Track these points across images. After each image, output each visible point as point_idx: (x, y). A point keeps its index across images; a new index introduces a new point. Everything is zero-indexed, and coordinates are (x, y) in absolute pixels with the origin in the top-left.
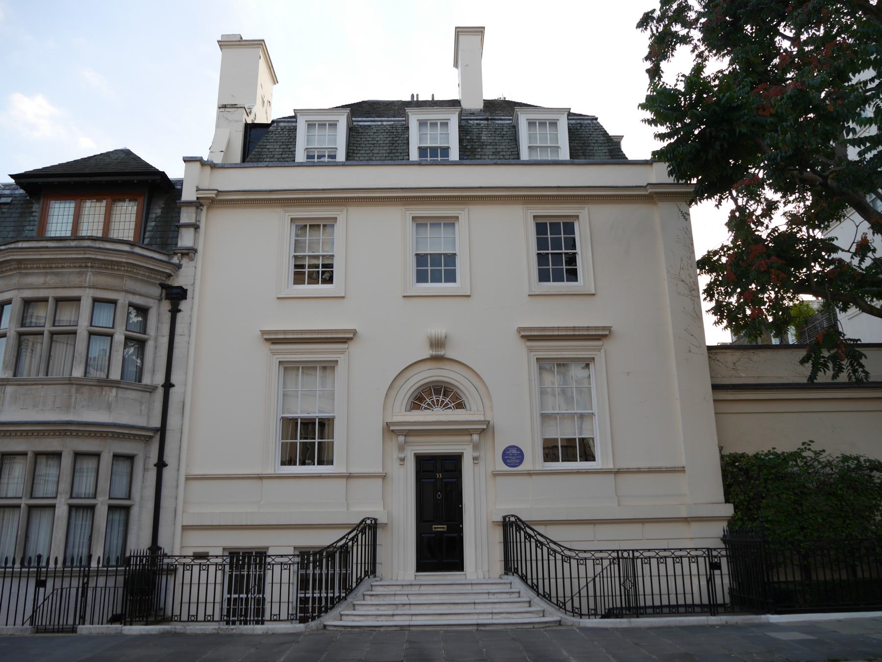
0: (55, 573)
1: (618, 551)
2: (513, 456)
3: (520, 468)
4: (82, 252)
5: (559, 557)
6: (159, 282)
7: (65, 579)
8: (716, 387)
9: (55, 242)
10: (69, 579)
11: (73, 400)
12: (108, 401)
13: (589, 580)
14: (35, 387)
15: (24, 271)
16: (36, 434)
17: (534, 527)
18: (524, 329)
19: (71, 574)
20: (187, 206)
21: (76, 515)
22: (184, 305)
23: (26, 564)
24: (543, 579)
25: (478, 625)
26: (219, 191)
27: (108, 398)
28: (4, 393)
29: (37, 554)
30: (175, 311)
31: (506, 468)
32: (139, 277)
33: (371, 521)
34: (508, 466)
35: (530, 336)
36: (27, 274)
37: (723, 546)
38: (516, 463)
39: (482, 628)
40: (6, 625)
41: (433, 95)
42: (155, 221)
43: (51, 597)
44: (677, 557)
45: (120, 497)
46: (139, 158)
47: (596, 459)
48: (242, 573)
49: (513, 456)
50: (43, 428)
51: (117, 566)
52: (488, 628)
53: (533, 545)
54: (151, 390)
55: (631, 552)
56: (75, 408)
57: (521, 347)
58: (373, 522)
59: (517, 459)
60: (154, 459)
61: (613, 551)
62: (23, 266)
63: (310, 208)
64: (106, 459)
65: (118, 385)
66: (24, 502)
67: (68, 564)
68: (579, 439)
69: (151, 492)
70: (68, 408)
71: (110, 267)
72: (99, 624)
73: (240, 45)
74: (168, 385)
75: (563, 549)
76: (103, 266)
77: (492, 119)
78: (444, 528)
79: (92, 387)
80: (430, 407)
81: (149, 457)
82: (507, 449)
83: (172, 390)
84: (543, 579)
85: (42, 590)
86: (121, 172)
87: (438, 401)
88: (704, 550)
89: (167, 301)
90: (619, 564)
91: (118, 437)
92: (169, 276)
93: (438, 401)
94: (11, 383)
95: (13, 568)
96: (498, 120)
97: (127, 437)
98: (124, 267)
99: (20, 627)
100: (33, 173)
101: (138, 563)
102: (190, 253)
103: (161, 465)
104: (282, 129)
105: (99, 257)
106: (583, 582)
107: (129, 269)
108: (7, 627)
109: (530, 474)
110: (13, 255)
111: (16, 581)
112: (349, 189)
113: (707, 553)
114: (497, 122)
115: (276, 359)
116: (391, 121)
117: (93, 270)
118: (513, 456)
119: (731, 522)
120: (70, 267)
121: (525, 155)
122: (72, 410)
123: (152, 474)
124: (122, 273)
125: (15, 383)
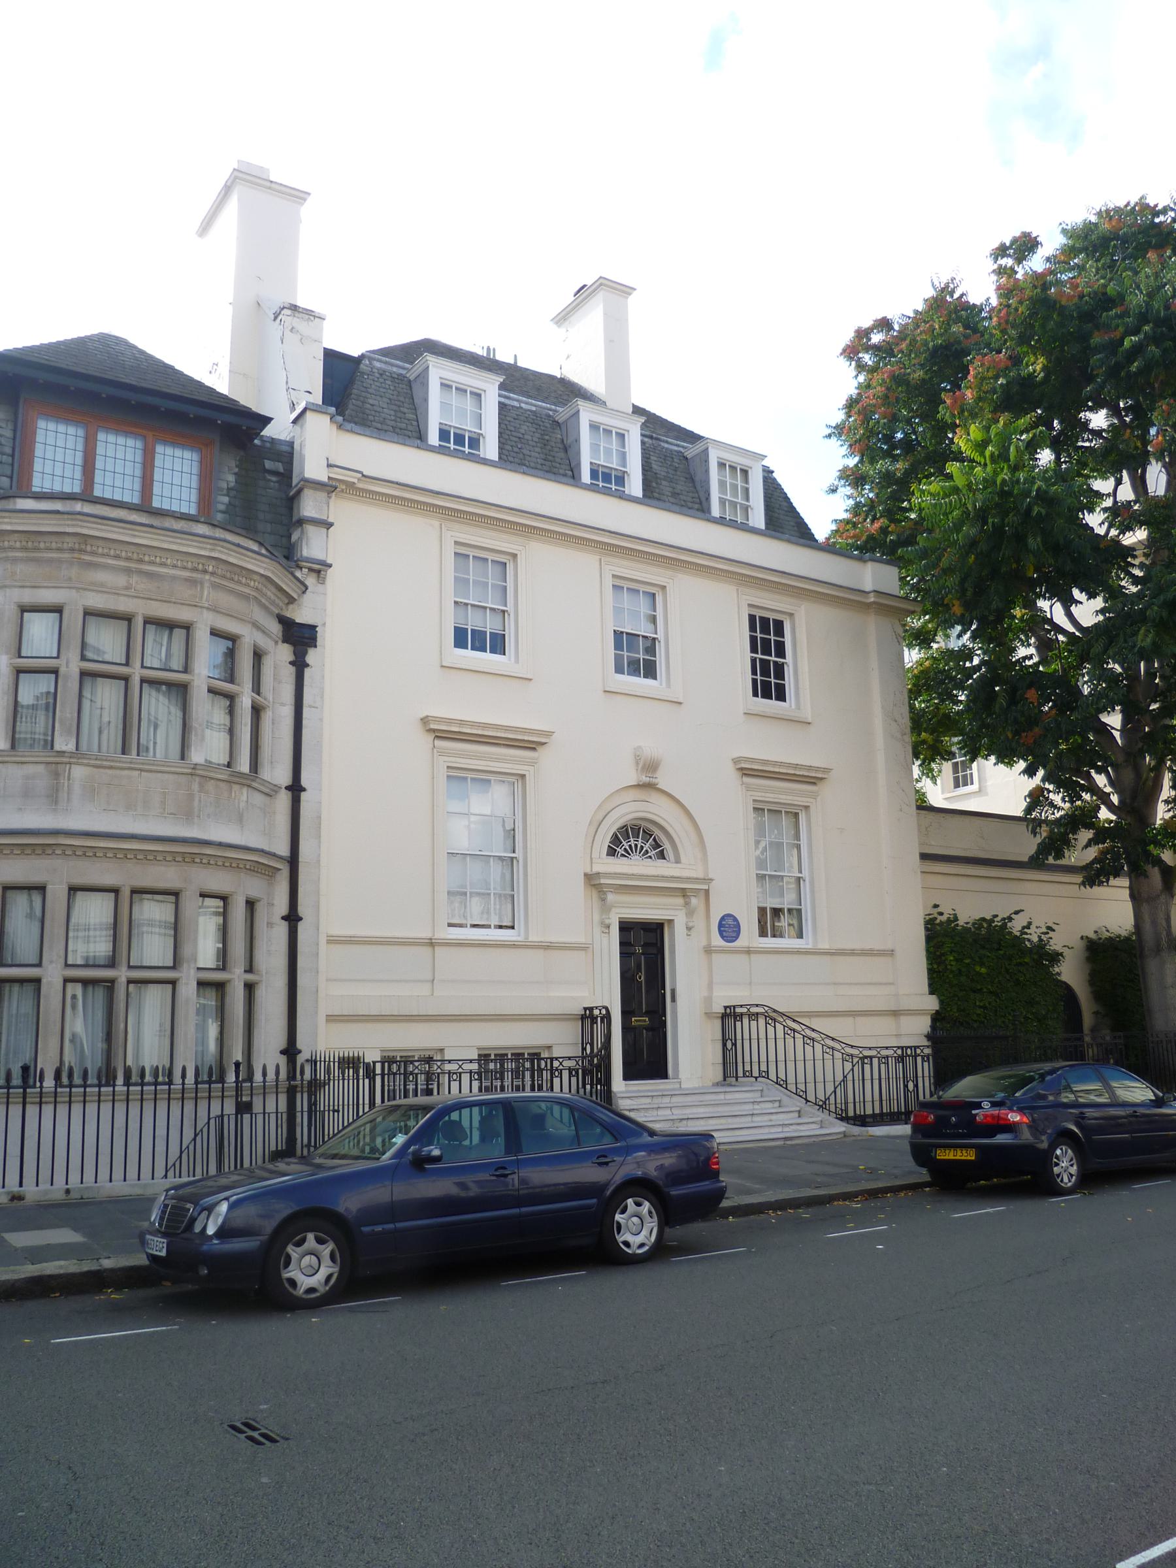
0: (169, 1094)
1: (902, 1048)
2: (730, 927)
3: (737, 944)
4: (209, 546)
5: (838, 1055)
6: (277, 612)
8: (924, 857)
9: (145, 514)
11: (196, 803)
12: (239, 807)
13: (837, 1084)
14: (126, 772)
15: (87, 558)
19: (99, 1098)
20: (315, 489)
22: (312, 656)
23: (65, 1081)
24: (923, 1077)
25: (786, 1139)
26: (363, 476)
27: (239, 803)
28: (69, 779)
29: (234, 1061)
30: (300, 665)
31: (722, 943)
32: (263, 601)
33: (600, 1010)
34: (725, 940)
35: (748, 771)
37: (926, 1043)
38: (732, 937)
39: (789, 1142)
40: (153, 1179)
41: (515, 356)
42: (228, 495)
43: (205, 1130)
44: (866, 1057)
45: (31, 962)
46: (172, 368)
48: (430, 1087)
49: (729, 928)
50: (134, 847)
51: (100, 1086)
52: (794, 1142)
53: (799, 1042)
55: (549, 1061)
56: (199, 817)
58: (604, 1012)
59: (734, 931)
60: (282, 907)
61: (899, 1047)
62: (89, 548)
63: (504, 536)
65: (249, 782)
67: (65, 1081)
68: (771, 908)
69: (281, 962)
70: (188, 815)
71: (236, 578)
72: (189, 1176)
73: (270, 188)
74: (296, 788)
75: (843, 1045)
76: (228, 575)
77: (657, 439)
78: (645, 1021)
79: (218, 782)
80: (627, 853)
81: (273, 905)
82: (723, 919)
83: (303, 795)
84: (923, 1077)
85: (247, 1117)
86: (187, 398)
87: (642, 848)
88: (577, 1059)
89: (286, 645)
90: (871, 1064)
91: (23, 853)
92: (291, 600)
93: (642, 848)
94: (85, 761)
96: (664, 441)
98: (254, 581)
100: (14, 354)
101: (386, 1072)
102: (320, 569)
103: (292, 918)
104: (381, 375)
105: (231, 560)
106: (830, 1089)
107: (30, 544)
108: (97, 1185)
109: (748, 952)
110: (82, 527)
112: (544, 516)
113: (580, 1063)
114: (662, 444)
115: (442, 763)
116: (532, 404)
117: (212, 579)
118: (729, 928)
119: (937, 1018)
120: (175, 566)
121: (716, 511)
122: (196, 819)
123: (282, 929)
124: (247, 590)
125: (93, 762)
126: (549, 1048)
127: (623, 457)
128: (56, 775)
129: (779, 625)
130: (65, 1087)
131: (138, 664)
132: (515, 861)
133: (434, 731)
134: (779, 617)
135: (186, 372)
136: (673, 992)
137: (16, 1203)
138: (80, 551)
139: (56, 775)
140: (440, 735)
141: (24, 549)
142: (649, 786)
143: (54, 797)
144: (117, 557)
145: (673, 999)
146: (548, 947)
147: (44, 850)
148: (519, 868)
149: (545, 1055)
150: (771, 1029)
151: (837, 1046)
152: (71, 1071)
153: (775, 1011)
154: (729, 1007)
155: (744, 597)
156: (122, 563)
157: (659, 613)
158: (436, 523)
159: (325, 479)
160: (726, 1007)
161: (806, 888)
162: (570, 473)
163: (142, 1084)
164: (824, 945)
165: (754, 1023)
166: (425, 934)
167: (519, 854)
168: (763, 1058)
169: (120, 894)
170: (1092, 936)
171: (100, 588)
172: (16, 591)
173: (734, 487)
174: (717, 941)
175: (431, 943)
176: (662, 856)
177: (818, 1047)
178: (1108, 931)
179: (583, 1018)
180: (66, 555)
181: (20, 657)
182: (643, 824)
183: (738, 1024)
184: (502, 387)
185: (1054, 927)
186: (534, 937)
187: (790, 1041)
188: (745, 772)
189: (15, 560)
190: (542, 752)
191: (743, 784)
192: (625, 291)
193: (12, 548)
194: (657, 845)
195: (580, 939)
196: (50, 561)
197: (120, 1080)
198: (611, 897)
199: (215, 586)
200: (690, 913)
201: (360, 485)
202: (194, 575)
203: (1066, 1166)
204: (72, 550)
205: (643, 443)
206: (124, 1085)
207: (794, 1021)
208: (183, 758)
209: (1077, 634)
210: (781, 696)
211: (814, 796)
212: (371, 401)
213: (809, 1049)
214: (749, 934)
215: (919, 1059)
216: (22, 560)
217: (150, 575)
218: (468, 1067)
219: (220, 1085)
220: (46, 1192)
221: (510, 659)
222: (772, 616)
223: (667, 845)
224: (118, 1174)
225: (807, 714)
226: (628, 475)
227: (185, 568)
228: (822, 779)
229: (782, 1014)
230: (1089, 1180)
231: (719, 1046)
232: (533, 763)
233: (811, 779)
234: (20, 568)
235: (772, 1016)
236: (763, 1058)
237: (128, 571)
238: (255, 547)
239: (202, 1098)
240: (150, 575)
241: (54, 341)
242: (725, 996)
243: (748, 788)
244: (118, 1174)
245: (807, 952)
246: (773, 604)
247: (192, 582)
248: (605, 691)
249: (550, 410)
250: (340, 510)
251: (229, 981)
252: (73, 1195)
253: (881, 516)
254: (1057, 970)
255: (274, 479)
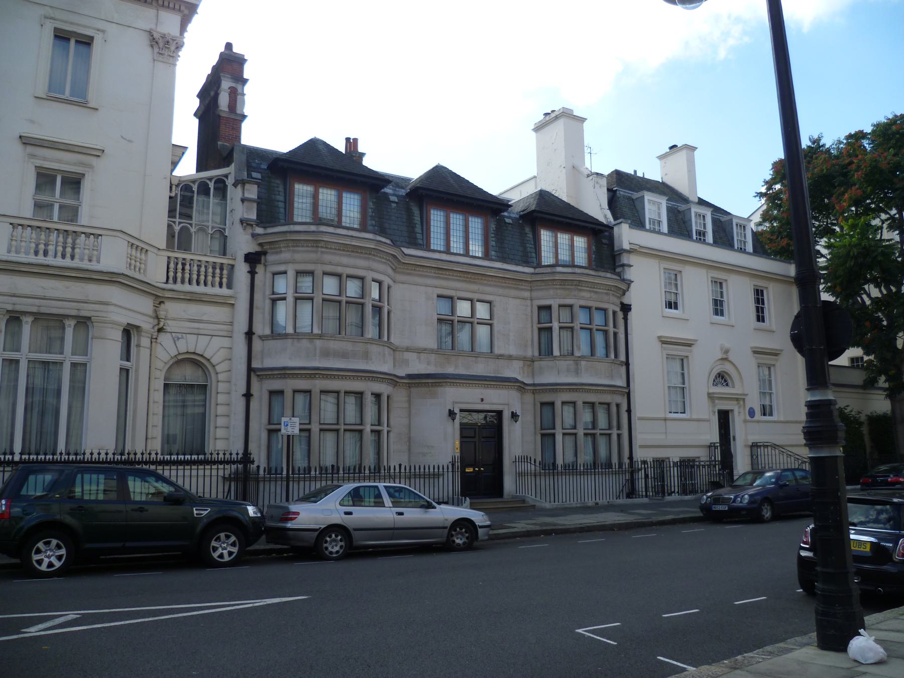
7: (323, 482)
10: (308, 482)
15: (579, 287)
16: (556, 391)
17: (786, 448)
18: (755, 347)
21: (323, 435)
23: (357, 471)
30: (626, 319)
31: (750, 419)
35: (756, 352)
36: (581, 290)
47: (773, 415)
49: (752, 413)
53: (785, 457)
54: (394, 349)
57: (658, 345)
63: (675, 264)
64: (288, 395)
66: (342, 427)
67: (567, 468)
71: (379, 255)
74: (627, 364)
94: (326, 338)
95: (364, 473)
97: (291, 376)
99: (569, 503)
103: (629, 411)
109: (758, 422)
111: (273, 484)
115: (665, 352)
121: (648, 227)
126: (699, 457)
127: (659, 214)
128: (577, 364)
129: (762, 291)
130: (373, 473)
131: (345, 296)
132: (685, 389)
133: (662, 341)
134: (762, 289)
135: (485, 189)
136: (734, 438)
137: (597, 505)
138: (579, 285)
139: (577, 364)
140: (664, 342)
141: (561, 285)
142: (726, 359)
143: (577, 372)
144: (588, 287)
145: (734, 439)
146: (698, 420)
147: (576, 390)
148: (687, 392)
149: (697, 460)
150: (773, 451)
151: (800, 458)
152: (549, 465)
153: (775, 445)
154: (755, 443)
155: (709, 274)
156: (588, 289)
157: (679, 283)
158: (657, 261)
159: (629, 249)
160: (753, 443)
161: (774, 397)
162: (687, 233)
163: (349, 473)
164: (782, 419)
165: (766, 449)
166: (663, 416)
167: (686, 385)
168: (763, 462)
169: (312, 393)
170: (869, 414)
171: (583, 298)
172: (558, 300)
173: (700, 223)
174: (748, 418)
175: (665, 419)
176: (727, 385)
177: (792, 458)
178: (876, 412)
179: (710, 447)
180: (573, 287)
181: (296, 293)
182: (722, 373)
183: (759, 450)
184: (667, 200)
185: (861, 411)
186: (694, 417)
187: (781, 457)
188: (755, 352)
189: (556, 288)
190: (693, 348)
191: (662, 347)
192: (693, 149)
193: (556, 285)
194: (725, 381)
195: (706, 417)
196: (569, 289)
197: (341, 472)
198: (717, 401)
199: (613, 295)
200: (740, 407)
201: (639, 250)
202: (608, 292)
203: (767, 513)
204: (576, 285)
205: (712, 217)
206: (319, 474)
207: (783, 448)
208: (607, 357)
209: (883, 285)
210: (763, 321)
211: (777, 360)
212: (624, 210)
213: (789, 459)
214: (758, 416)
215: (701, 467)
216: (559, 289)
217: (596, 292)
218: (707, 463)
219: (337, 475)
220: (557, 505)
221: (680, 312)
222: (760, 289)
223: (729, 381)
224: (572, 499)
225: (774, 328)
226: (661, 222)
227: (605, 289)
228: (693, 344)
229: (778, 446)
230: (776, 518)
231: (750, 458)
232: (691, 351)
233: (775, 354)
234: (559, 291)
235: (774, 446)
236: (763, 462)
237: (590, 291)
238: (388, 241)
239: (307, 481)
240: (596, 292)
241: (288, 151)
242: (753, 438)
243: (756, 358)
244: (572, 499)
245: (775, 422)
246: (761, 283)
247: (607, 294)
248: (711, 323)
249: (675, 205)
250: (632, 259)
251: (382, 430)
252: (610, 503)
253: (785, 237)
254: (862, 429)
255: (606, 246)
